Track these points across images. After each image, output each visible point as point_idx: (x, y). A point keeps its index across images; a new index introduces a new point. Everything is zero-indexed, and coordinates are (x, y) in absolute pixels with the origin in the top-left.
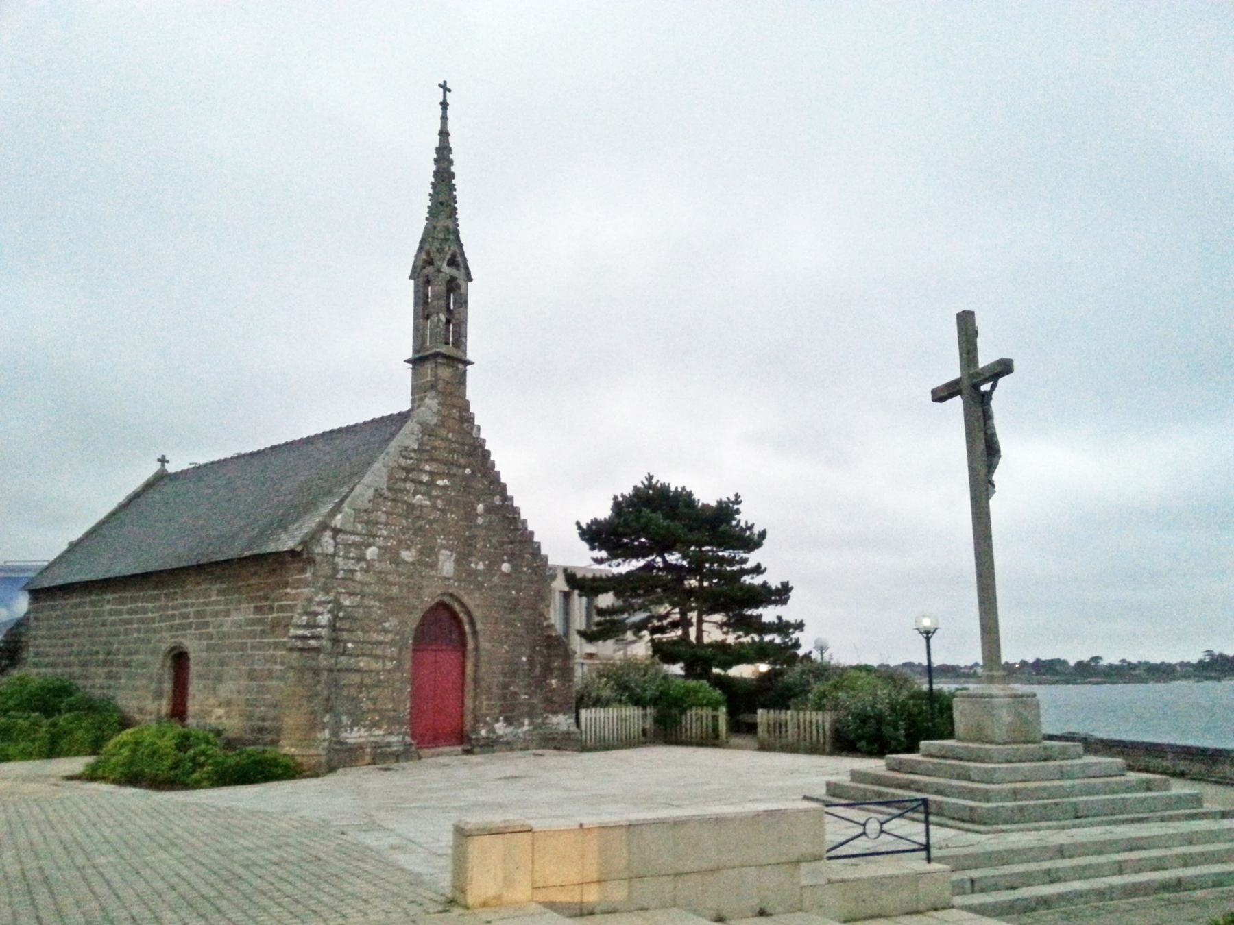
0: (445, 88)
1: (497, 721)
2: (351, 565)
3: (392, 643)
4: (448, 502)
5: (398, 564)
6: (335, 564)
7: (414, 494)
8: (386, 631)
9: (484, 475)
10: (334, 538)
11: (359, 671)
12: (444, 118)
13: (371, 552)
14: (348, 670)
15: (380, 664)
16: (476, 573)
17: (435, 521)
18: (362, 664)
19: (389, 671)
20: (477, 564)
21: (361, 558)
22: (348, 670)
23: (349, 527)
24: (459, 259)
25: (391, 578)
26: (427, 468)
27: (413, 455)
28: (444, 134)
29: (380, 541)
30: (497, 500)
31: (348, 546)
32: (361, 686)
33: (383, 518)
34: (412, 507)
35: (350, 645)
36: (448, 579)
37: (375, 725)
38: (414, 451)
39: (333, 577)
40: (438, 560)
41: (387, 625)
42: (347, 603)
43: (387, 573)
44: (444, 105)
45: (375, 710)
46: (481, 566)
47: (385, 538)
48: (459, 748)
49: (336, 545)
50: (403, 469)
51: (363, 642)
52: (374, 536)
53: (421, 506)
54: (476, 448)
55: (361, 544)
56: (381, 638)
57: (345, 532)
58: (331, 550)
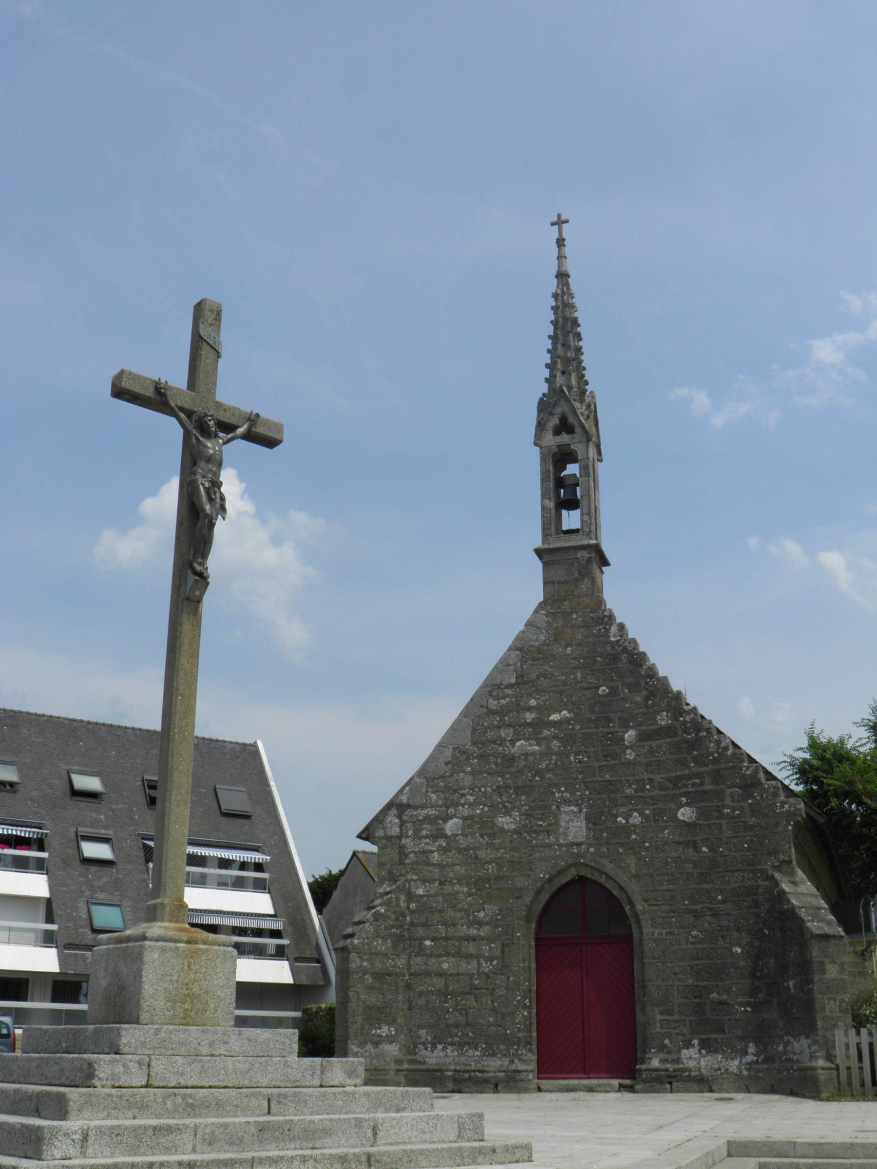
0: (205, 430)
1: (688, 1045)
2: (425, 845)
3: (489, 940)
4: (570, 740)
5: (492, 836)
6: (402, 848)
7: (513, 742)
8: (481, 924)
9: (634, 687)
10: (399, 817)
11: (440, 975)
12: (561, 257)
13: (451, 826)
14: (428, 974)
15: (474, 963)
16: (627, 830)
17: (548, 770)
18: (445, 966)
19: (487, 975)
20: (627, 817)
21: (440, 834)
22: (428, 974)
23: (418, 801)
24: (571, 419)
25: (482, 854)
26: (533, 702)
27: (509, 691)
28: (562, 276)
29: (465, 811)
30: (663, 719)
31: (418, 824)
32: (444, 994)
33: (468, 780)
34: (512, 759)
35: (428, 943)
36: (579, 844)
37: (472, 1044)
38: (510, 686)
39: (401, 862)
40: (557, 823)
41: (481, 915)
42: (420, 892)
43: (475, 849)
44: (560, 242)
45: (467, 1024)
46: (636, 819)
47: (471, 805)
48: (616, 1082)
49: (402, 823)
50: (494, 713)
51: (446, 939)
52: (456, 805)
53: (527, 755)
54: (615, 658)
55: (438, 817)
56: (473, 932)
57: (415, 807)
58: (396, 831)
